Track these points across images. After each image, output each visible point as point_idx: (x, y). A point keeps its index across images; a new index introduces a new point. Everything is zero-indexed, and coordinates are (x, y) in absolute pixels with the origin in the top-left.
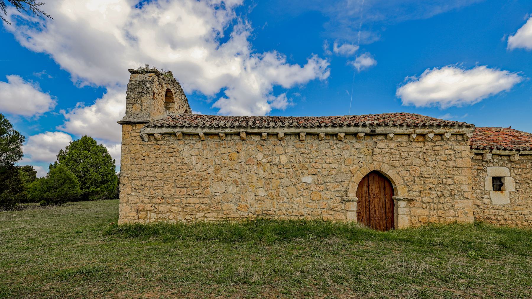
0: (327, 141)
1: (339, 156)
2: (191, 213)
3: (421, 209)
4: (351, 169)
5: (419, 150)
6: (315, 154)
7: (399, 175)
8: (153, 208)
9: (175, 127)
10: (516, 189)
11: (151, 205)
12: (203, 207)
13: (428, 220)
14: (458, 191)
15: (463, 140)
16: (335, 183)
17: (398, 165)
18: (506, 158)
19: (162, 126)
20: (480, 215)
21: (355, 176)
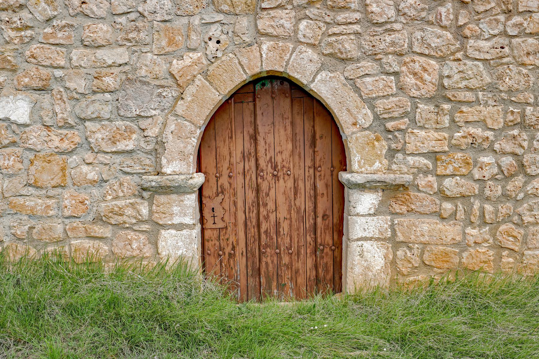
1: (133, 16)
3: (436, 220)
7: (357, 90)
16: (119, 123)
17: (355, 54)
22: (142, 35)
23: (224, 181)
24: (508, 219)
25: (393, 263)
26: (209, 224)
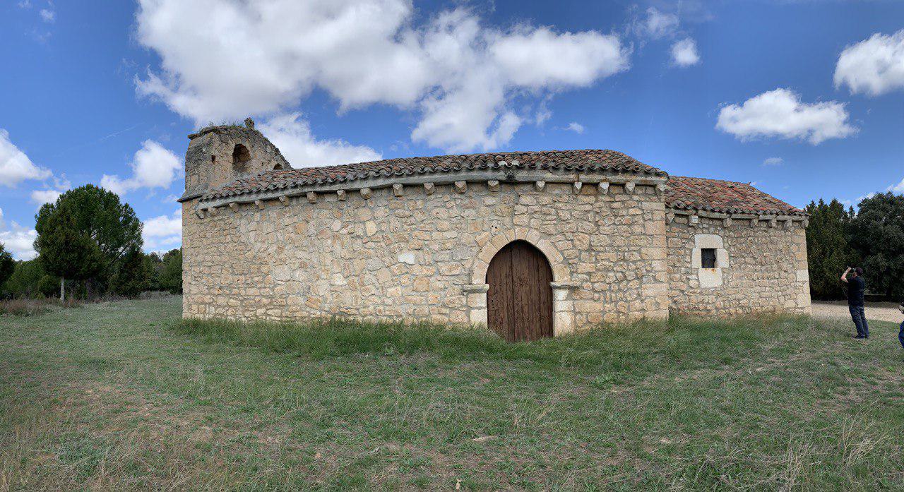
0: (438, 196)
1: (459, 218)
2: (251, 309)
3: (592, 301)
4: (478, 238)
5: (588, 207)
6: (419, 217)
7: (556, 247)
8: (211, 301)
9: (228, 196)
10: (730, 265)
11: (209, 296)
12: (265, 300)
13: (601, 319)
14: (646, 270)
15: (655, 194)
16: (453, 263)
17: (554, 233)
18: (718, 223)
19: (214, 198)
20: (685, 305)
21: (483, 251)
22: (463, 225)
23: (498, 287)
24: (621, 299)
25: (575, 322)
26: (491, 308)
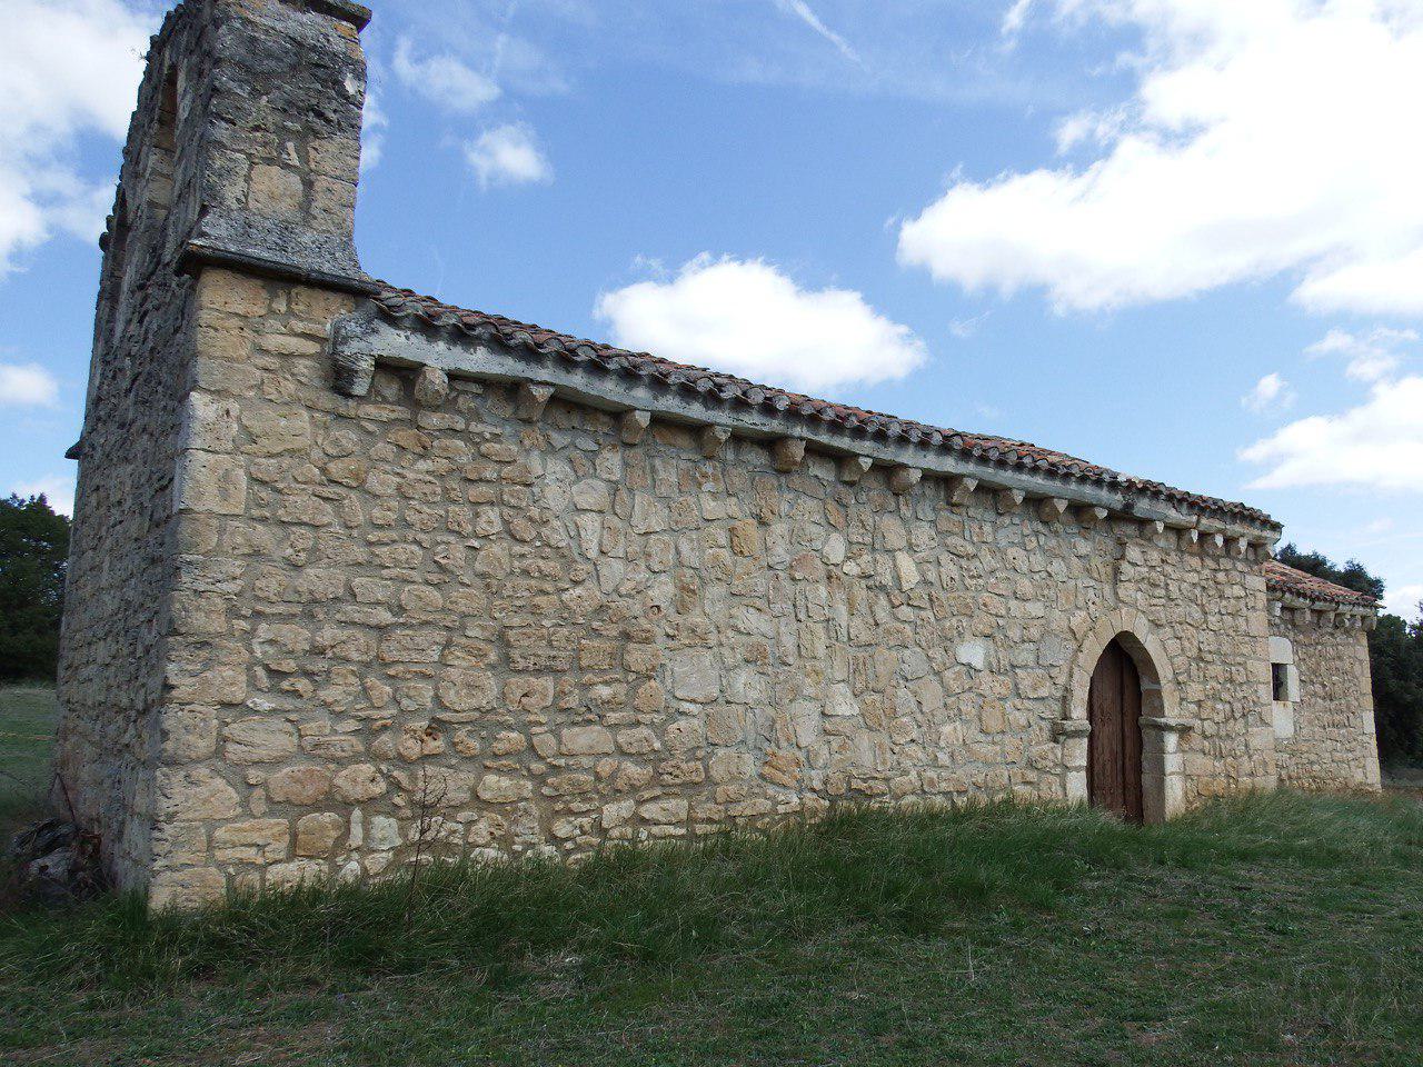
6: (988, 561)
8: (380, 787)
12: (632, 770)
21: (1084, 648)
